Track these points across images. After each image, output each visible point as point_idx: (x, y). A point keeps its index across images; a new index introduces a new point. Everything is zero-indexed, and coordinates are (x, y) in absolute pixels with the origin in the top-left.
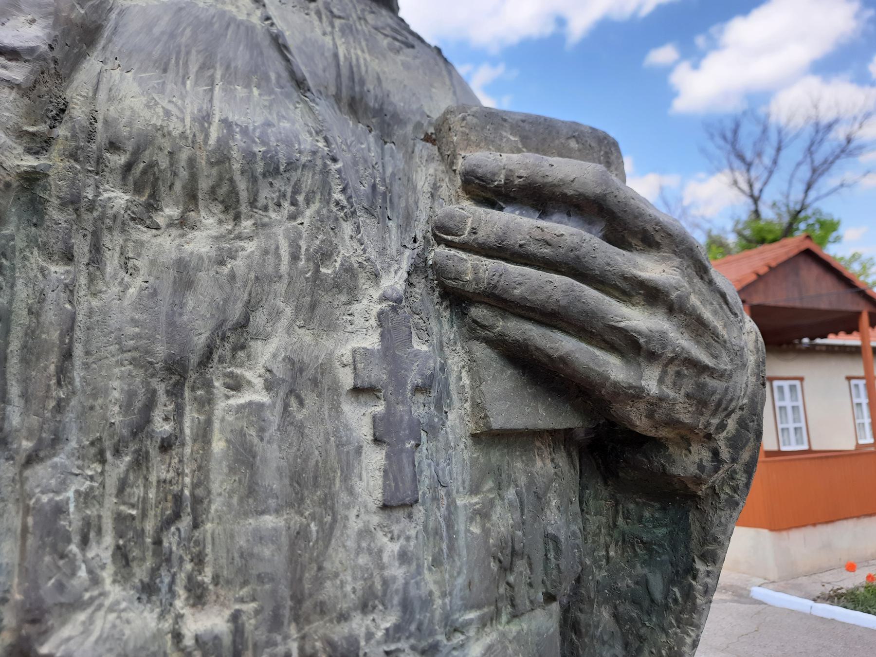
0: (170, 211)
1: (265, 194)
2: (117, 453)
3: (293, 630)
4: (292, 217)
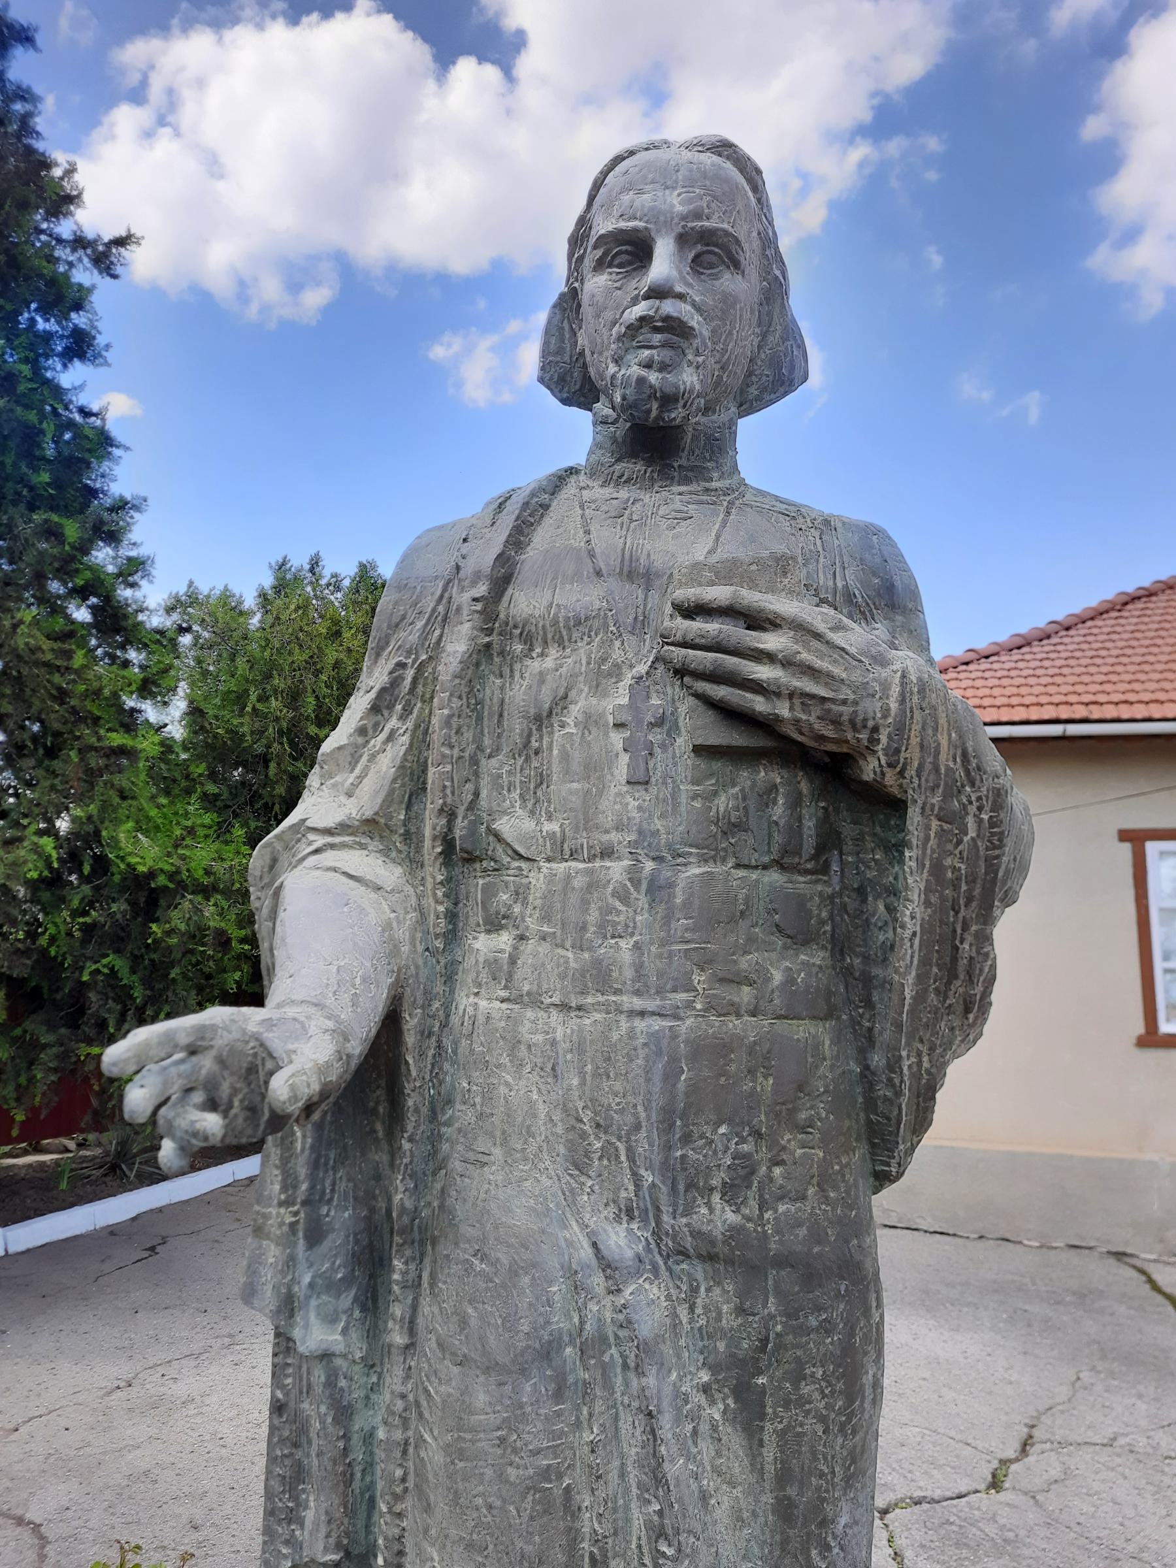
0: (538, 650)
1: (575, 635)
2: (520, 755)
3: (584, 834)
4: (589, 644)
